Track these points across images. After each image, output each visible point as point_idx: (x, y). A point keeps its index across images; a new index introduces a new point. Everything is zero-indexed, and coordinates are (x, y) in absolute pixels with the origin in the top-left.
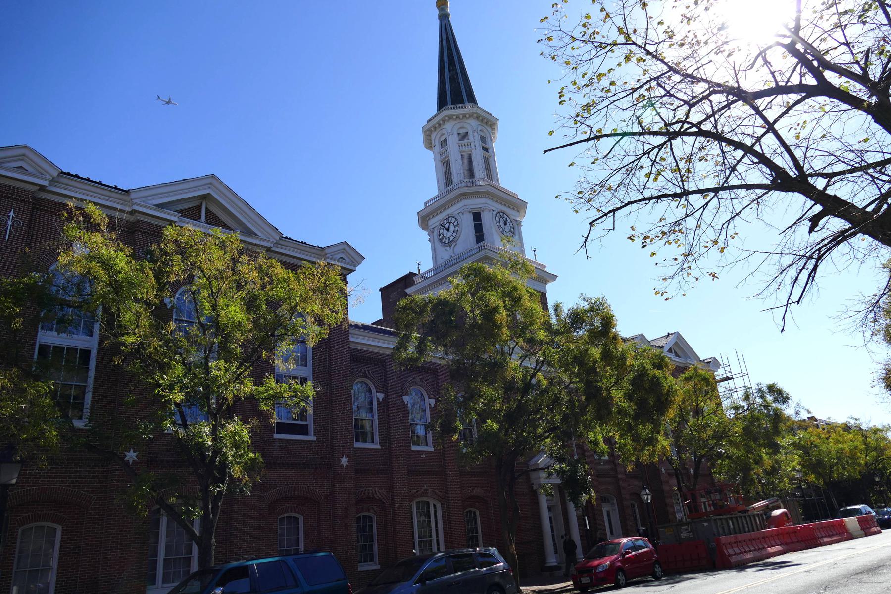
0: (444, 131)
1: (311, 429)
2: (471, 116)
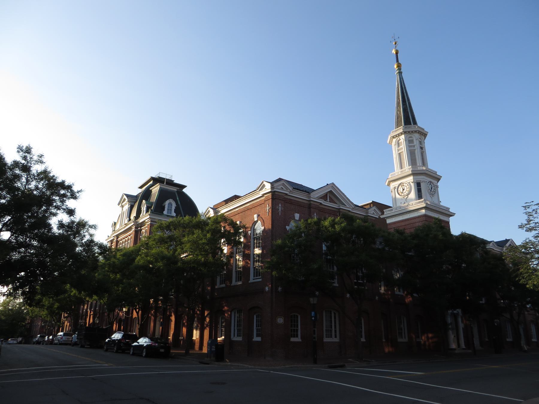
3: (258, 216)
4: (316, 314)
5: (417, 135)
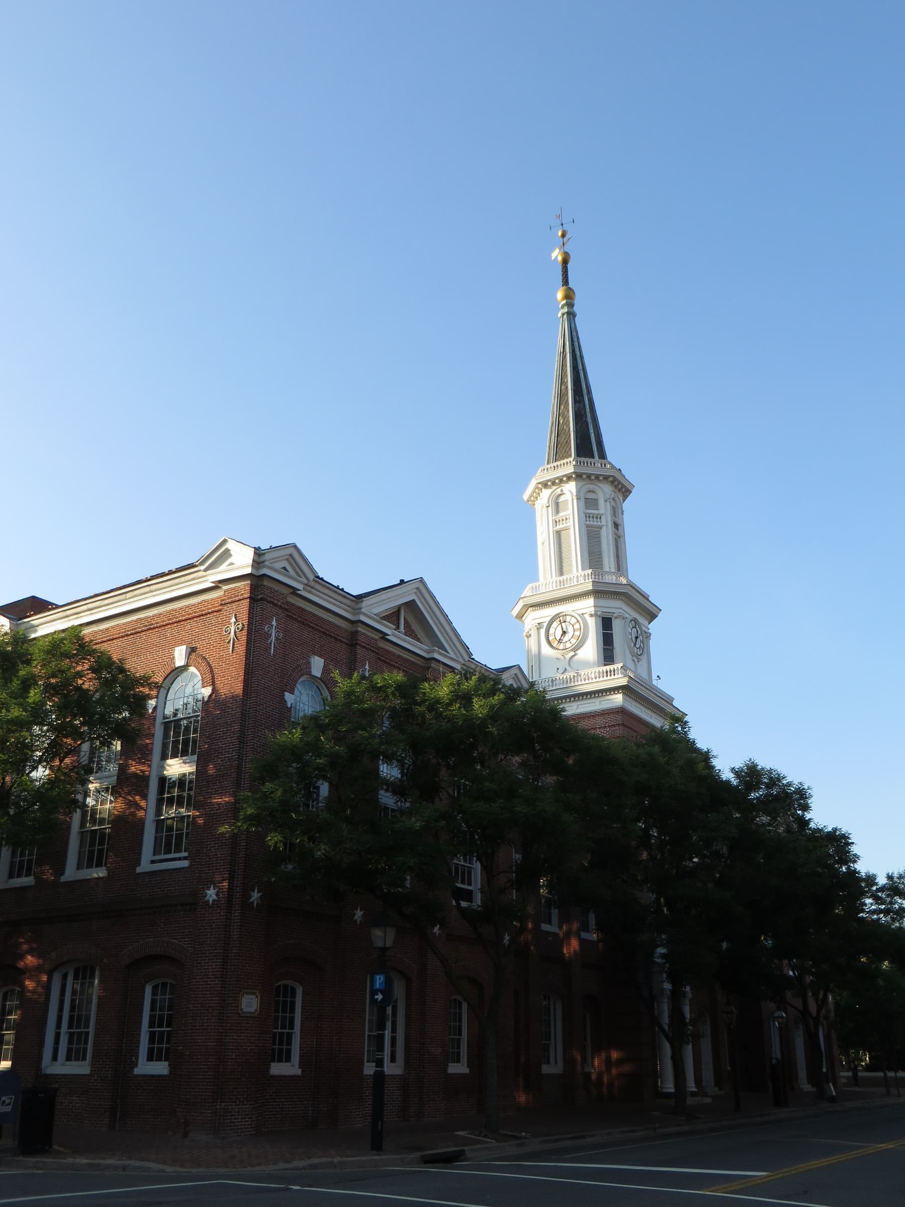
3: (192, 650)
4: (389, 983)
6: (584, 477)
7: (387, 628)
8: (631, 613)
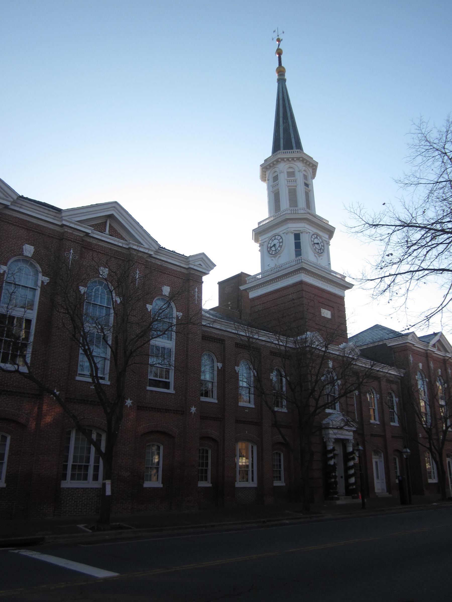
0: (276, 169)
1: (172, 385)
2: (298, 159)
5: (300, 165)
6: (285, 160)
7: (435, 350)
8: (313, 230)
